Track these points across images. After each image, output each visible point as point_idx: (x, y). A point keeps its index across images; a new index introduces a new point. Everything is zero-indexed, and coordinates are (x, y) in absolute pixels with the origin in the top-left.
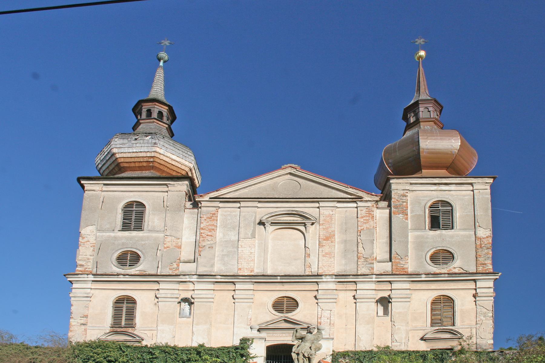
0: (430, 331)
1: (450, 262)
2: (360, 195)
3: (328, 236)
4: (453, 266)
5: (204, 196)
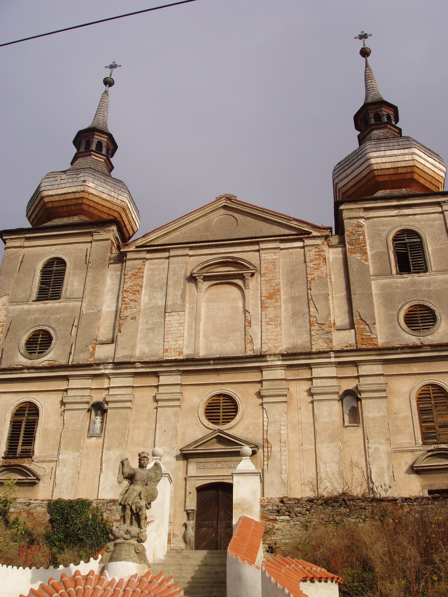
0: (422, 452)
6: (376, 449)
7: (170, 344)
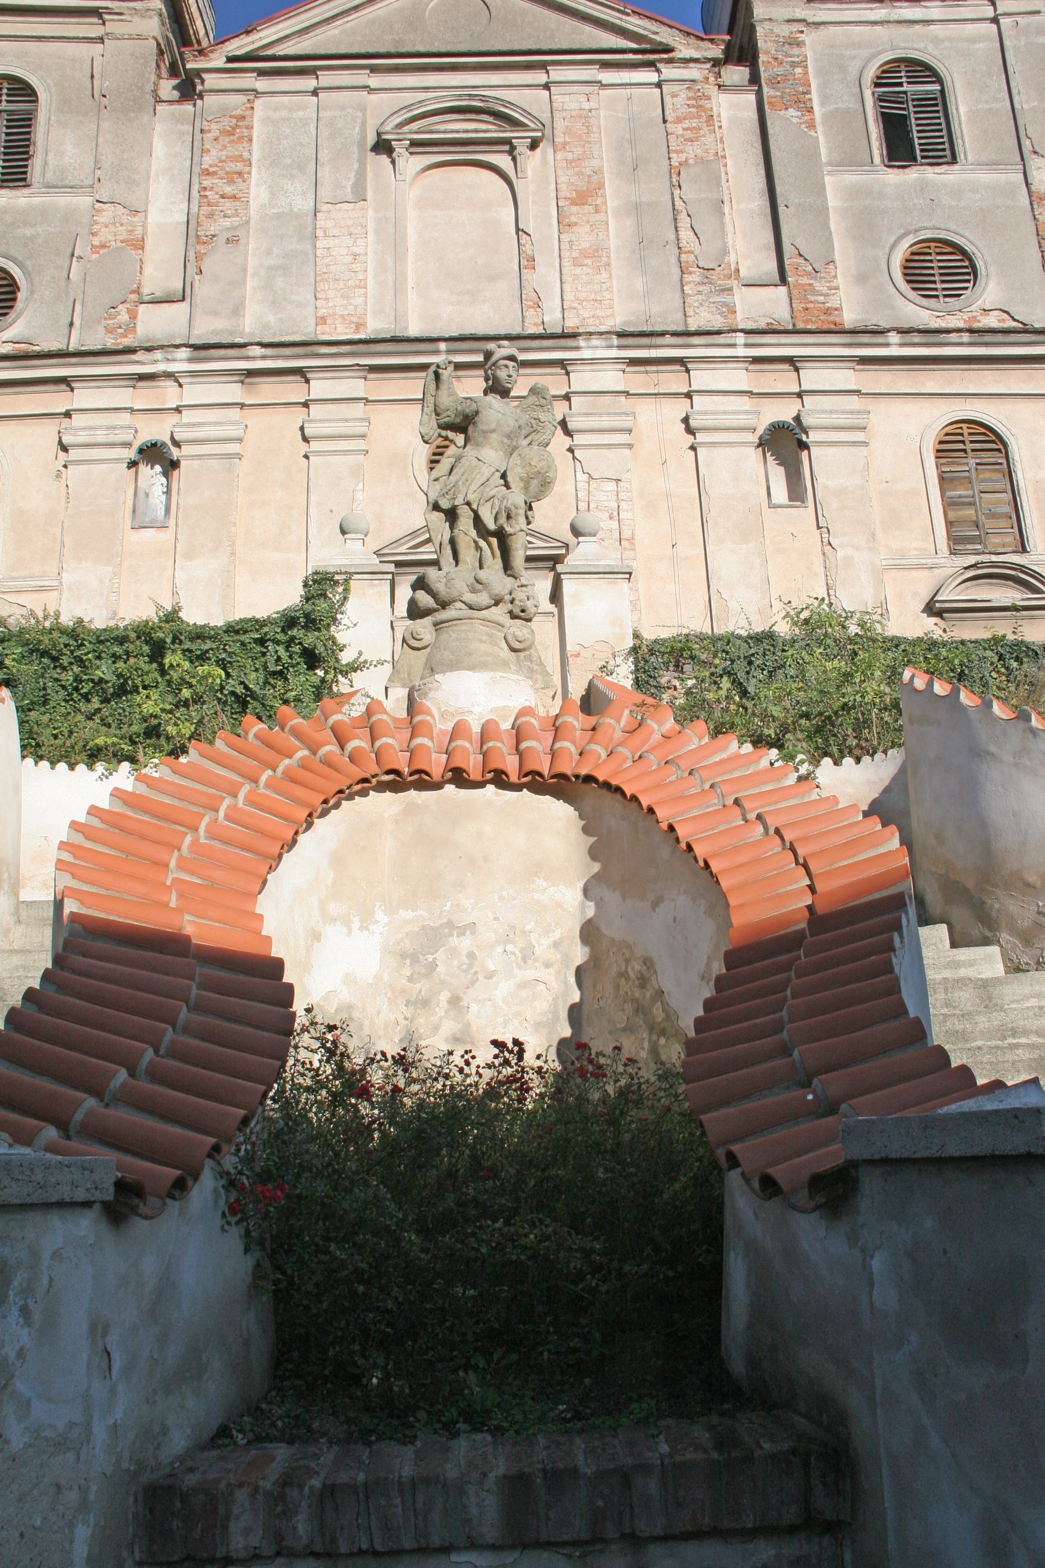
0: (950, 571)
1: (966, 288)
2: (664, 41)
3: (584, 188)
4: (980, 302)
5: (212, 52)
6: (848, 561)
7: (330, 304)
